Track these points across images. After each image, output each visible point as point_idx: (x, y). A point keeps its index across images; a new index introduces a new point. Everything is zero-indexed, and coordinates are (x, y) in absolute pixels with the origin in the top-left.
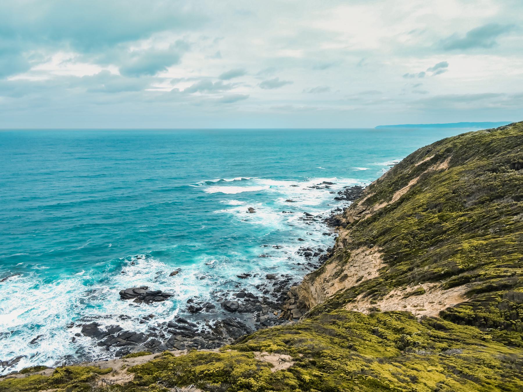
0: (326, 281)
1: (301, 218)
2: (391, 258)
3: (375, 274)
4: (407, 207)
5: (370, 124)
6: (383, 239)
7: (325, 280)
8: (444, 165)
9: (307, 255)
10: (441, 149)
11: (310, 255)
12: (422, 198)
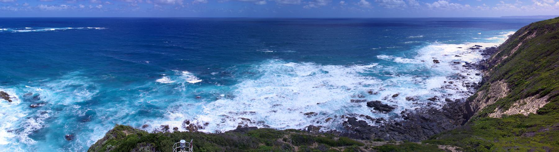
0: (479, 101)
1: (464, 66)
2: (512, 85)
3: (505, 95)
4: (517, 58)
5: (478, 19)
6: (507, 76)
7: (478, 100)
8: (533, 35)
9: (467, 86)
10: (532, 27)
11: (469, 86)
12: (524, 52)
